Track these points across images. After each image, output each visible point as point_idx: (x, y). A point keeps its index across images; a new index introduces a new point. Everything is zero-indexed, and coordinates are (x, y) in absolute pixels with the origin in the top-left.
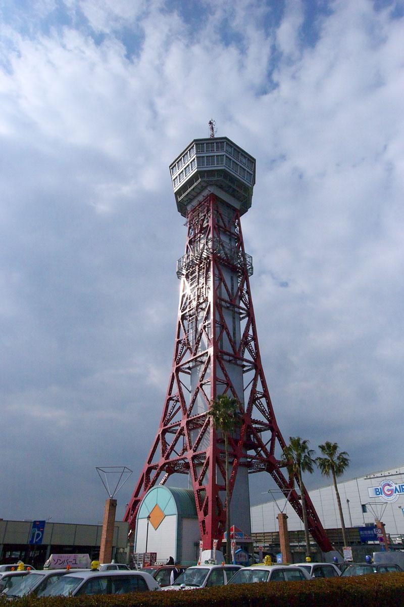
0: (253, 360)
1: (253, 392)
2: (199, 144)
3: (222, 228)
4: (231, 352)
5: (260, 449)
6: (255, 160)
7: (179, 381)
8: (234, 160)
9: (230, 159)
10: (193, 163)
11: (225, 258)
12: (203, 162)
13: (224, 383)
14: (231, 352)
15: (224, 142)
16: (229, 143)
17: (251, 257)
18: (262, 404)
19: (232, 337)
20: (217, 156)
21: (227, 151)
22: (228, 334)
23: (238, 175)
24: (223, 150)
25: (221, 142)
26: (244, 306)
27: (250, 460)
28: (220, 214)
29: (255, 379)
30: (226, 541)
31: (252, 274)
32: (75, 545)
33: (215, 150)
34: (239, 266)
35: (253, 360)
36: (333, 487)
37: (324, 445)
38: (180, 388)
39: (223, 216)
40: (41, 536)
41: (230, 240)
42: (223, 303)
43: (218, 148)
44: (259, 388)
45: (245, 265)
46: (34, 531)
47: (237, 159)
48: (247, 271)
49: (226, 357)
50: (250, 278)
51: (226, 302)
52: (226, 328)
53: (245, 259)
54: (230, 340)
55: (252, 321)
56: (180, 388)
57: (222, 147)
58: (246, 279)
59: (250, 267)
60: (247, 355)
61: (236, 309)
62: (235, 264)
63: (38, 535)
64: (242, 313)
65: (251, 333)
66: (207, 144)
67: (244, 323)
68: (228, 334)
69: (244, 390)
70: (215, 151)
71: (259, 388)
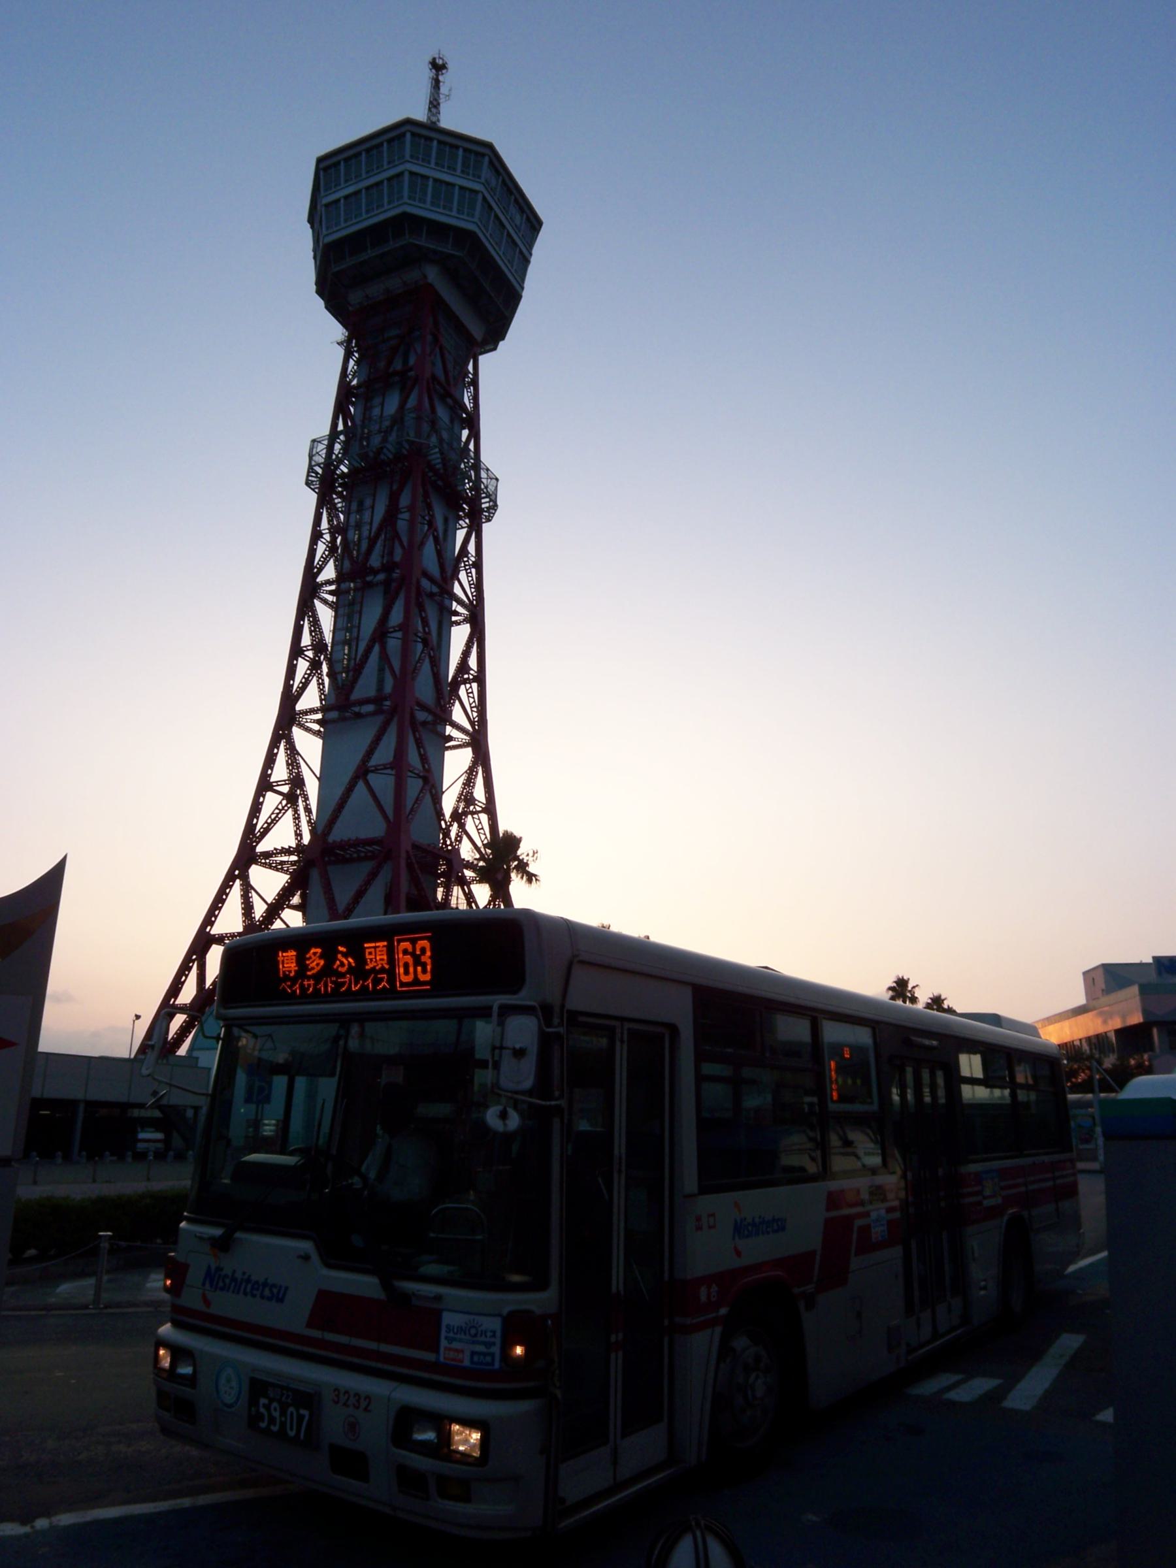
3: (439, 383)
6: (540, 223)
7: (293, 752)
8: (498, 212)
9: (490, 207)
10: (375, 152)
13: (419, 776)
15: (483, 155)
16: (527, 246)
17: (497, 479)
18: (277, 808)
21: (486, 184)
23: (498, 254)
24: (479, 177)
25: (477, 154)
28: (441, 348)
29: (471, 773)
31: (490, 521)
32: (46, 1096)
43: (465, 165)
50: (486, 527)
58: (476, 529)
65: (473, 662)
67: (459, 635)
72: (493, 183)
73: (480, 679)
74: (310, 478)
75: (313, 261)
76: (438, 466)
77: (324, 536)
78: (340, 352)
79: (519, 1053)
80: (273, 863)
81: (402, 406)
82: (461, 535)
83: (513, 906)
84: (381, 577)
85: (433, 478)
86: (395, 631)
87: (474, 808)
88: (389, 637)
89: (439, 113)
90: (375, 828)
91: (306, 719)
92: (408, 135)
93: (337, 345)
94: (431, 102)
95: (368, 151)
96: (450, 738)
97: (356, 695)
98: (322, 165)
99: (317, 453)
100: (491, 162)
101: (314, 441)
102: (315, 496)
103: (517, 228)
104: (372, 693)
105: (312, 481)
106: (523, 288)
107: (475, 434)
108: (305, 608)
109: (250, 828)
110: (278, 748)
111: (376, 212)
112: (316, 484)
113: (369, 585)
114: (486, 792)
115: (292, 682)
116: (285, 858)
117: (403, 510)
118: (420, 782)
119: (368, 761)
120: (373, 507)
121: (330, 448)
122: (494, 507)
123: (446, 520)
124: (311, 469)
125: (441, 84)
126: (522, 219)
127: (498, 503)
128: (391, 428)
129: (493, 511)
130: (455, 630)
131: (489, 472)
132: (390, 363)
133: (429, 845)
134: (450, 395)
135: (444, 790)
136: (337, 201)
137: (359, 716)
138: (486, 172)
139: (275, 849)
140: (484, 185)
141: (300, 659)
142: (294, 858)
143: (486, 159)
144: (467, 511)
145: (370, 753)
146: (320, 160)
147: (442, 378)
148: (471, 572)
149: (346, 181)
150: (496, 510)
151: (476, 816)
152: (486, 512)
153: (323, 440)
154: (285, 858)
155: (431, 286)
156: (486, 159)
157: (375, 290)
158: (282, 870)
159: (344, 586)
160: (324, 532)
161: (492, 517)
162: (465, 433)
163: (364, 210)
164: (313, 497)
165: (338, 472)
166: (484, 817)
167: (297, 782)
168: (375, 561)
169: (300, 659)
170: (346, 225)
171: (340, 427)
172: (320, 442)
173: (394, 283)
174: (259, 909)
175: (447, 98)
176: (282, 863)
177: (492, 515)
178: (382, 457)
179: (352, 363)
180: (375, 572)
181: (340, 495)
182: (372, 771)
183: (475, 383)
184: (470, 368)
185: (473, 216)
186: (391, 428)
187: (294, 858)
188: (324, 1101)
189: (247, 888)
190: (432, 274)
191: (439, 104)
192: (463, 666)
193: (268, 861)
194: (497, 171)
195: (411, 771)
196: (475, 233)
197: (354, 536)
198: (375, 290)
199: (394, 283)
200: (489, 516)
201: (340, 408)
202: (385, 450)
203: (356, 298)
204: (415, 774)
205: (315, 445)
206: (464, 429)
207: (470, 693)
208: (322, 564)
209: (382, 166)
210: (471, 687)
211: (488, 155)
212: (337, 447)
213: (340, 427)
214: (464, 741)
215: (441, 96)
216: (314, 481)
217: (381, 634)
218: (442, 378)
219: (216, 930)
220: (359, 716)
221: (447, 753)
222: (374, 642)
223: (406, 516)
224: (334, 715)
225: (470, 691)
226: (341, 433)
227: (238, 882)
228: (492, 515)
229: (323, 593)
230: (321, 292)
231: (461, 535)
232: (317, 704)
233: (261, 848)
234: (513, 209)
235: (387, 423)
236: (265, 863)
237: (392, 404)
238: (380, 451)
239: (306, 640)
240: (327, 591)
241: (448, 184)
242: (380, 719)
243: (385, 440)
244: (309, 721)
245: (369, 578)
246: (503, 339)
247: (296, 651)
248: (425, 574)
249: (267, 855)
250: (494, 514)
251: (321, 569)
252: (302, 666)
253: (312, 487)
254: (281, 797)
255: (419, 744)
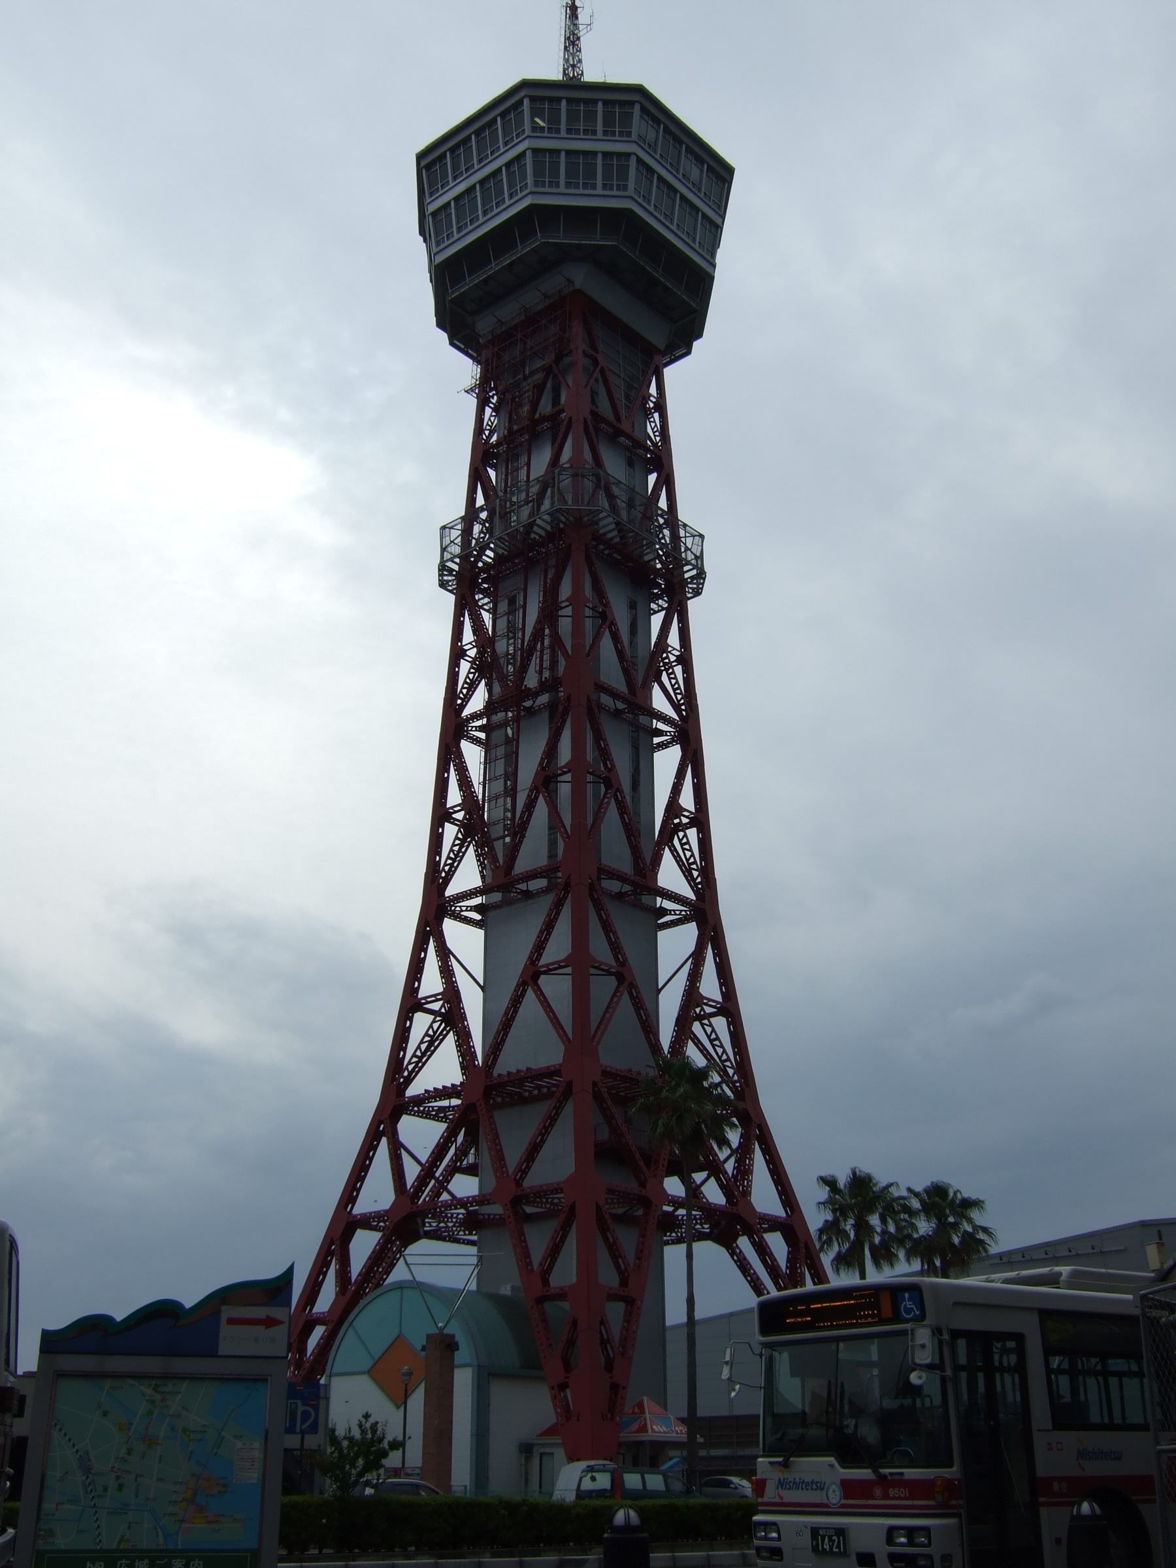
0: (691, 895)
1: (692, 996)
2: (542, 99)
4: (621, 686)
5: (699, 1177)
7: (444, 953)
9: (651, 170)
11: (617, 540)
12: (555, 172)
14: (621, 686)
15: (632, 103)
17: (702, 536)
19: (628, 799)
20: (606, 155)
22: (616, 637)
24: (629, 134)
25: (622, 103)
26: (671, 712)
27: (670, 1209)
29: (697, 958)
30: (694, 1175)
33: (600, 128)
34: (659, 566)
35: (691, 895)
36: (698, 1315)
37: (842, 1180)
38: (447, 973)
39: (612, 379)
40: (313, 1416)
41: (630, 464)
42: (606, 700)
43: (608, 121)
44: (710, 987)
45: (680, 563)
46: (293, 1406)
47: (675, 168)
48: (684, 583)
49: (614, 886)
50: (693, 605)
51: (615, 695)
52: (613, 623)
53: (675, 537)
54: (621, 654)
55: (693, 759)
56: (447, 973)
57: (627, 119)
58: (678, 610)
59: (694, 572)
60: (670, 876)
61: (643, 719)
62: (646, 558)
63: (305, 1415)
64: (660, 733)
66: (570, 101)
67: (666, 762)
68: (616, 637)
69: (659, 991)
70: (600, 135)
71: (710, 987)
72: (651, 135)
73: (700, 820)
74: (445, 578)
75: (431, 284)
76: (609, 536)
77: (468, 653)
78: (472, 402)
79: (923, 1346)
80: (433, 1111)
81: (555, 461)
82: (657, 621)
83: (666, 1177)
84: (544, 699)
85: (606, 552)
86: (564, 773)
87: (702, 1009)
88: (560, 782)
89: (580, 51)
90: (550, 1053)
91: (460, 907)
92: (526, 102)
93: (466, 394)
94: (567, 39)
95: (478, 133)
96: (664, 912)
97: (522, 865)
98: (423, 163)
99: (452, 542)
100: (644, 110)
101: (444, 528)
102: (453, 597)
103: (696, 187)
104: (542, 861)
105: (448, 581)
106: (714, 266)
107: (667, 480)
108: (449, 754)
109: (395, 1065)
110: (426, 951)
111: (496, 211)
112: (452, 585)
113: (531, 712)
114: (721, 985)
115: (438, 858)
116: (445, 1103)
117: (563, 605)
118: (612, 982)
119: (538, 959)
120: (524, 607)
121: (467, 532)
122: (701, 575)
123: (633, 606)
124: (442, 568)
125: (579, 10)
126: (702, 170)
127: (707, 568)
128: (541, 494)
129: (702, 581)
130: (659, 757)
131: (687, 528)
132: (535, 405)
133: (630, 1070)
134: (619, 433)
135: (660, 986)
136: (447, 205)
137: (527, 895)
138: (638, 123)
139: (426, 1091)
140: (637, 144)
141: (447, 824)
142: (456, 1102)
143: (637, 107)
144: (663, 586)
145: (540, 947)
146: (420, 157)
147: (610, 416)
148: (673, 673)
149: (455, 178)
150: (704, 579)
151: (706, 1022)
152: (690, 583)
153: (455, 525)
154: (445, 1103)
155: (580, 293)
156: (637, 107)
157: (509, 311)
158: (436, 1118)
159: (499, 717)
160: (465, 648)
161: (702, 589)
162: (652, 478)
163: (480, 212)
164: (451, 599)
165: (480, 564)
166: (720, 1023)
167: (452, 994)
168: (531, 681)
169: (447, 824)
170: (460, 235)
171: (480, 501)
172: (452, 528)
173: (532, 298)
174: (412, 1172)
175: (589, 27)
176: (442, 1109)
177: (701, 586)
178: (533, 536)
179: (488, 411)
180: (535, 694)
181: (486, 593)
182: (545, 973)
183: (661, 407)
184: (653, 390)
185: (625, 188)
186: (541, 494)
187: (456, 1102)
188: (842, 1383)
189: (396, 1148)
190: (580, 277)
191: (578, 39)
192: (673, 807)
193: (422, 1109)
194: (657, 122)
195: (593, 967)
196: (630, 211)
197: (508, 648)
198: (509, 311)
199: (532, 298)
200: (698, 588)
201: (477, 476)
202: (535, 528)
203: (485, 325)
204: (602, 970)
205: (447, 534)
206: (651, 473)
207: (685, 844)
208: (468, 692)
209: (473, 165)
210: (685, 835)
211: (638, 102)
212: (477, 528)
213: (480, 501)
214: (683, 913)
215: (581, 27)
216: (450, 581)
217: (546, 781)
218: (610, 416)
219: (362, 1207)
220: (527, 895)
221: (662, 935)
222: (538, 792)
223: (568, 611)
224: (497, 897)
225: (685, 840)
226: (482, 509)
227: (384, 1140)
228: (701, 586)
229: (471, 730)
230: (441, 324)
231: (657, 621)
232: (477, 882)
233: (415, 1089)
234: (686, 163)
235: (534, 489)
236: (419, 1111)
237: (540, 462)
238: (530, 526)
239: (454, 797)
240: (476, 727)
241: (586, 153)
242: (550, 899)
243: (534, 513)
244: (464, 909)
245: (528, 704)
246: (699, 335)
247: (441, 815)
248: (601, 688)
249: (419, 1100)
250: (703, 584)
251: (467, 698)
252: (450, 832)
253: (450, 588)
254: (431, 1017)
255: (607, 927)
